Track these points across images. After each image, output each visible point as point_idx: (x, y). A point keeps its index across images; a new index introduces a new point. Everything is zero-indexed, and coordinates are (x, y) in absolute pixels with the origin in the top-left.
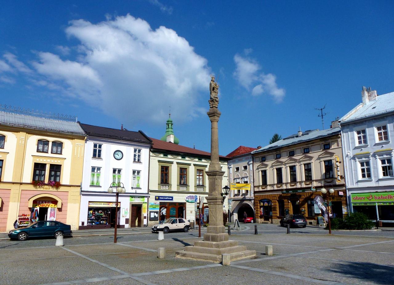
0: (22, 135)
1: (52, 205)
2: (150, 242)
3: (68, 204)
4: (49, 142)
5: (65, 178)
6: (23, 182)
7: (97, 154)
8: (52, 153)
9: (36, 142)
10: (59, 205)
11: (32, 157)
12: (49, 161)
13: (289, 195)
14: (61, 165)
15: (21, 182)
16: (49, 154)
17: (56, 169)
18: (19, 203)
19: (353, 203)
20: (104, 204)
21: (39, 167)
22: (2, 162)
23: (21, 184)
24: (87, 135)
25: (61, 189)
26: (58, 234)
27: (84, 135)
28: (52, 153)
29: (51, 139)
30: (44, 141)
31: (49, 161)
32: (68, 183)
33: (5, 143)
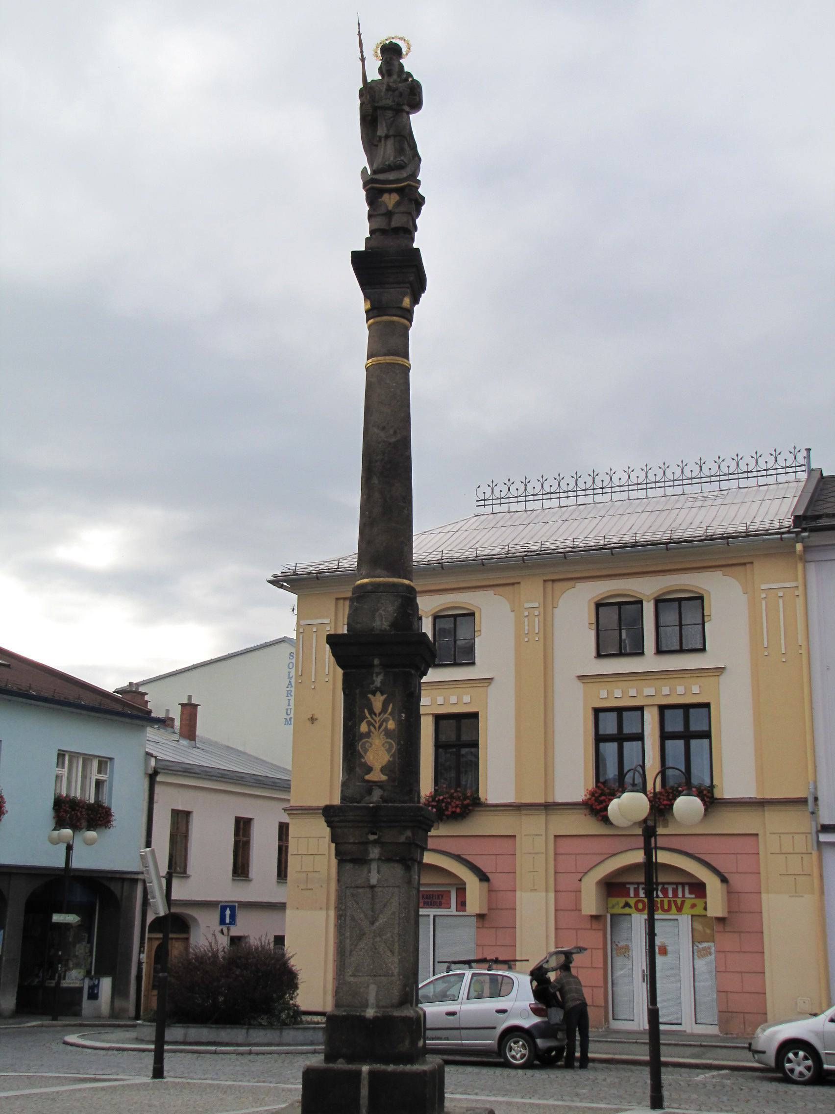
0: (531, 593)
1: (693, 906)
2: (28, 1096)
3: (764, 896)
4: (640, 602)
5: (736, 769)
6: (559, 799)
8: (659, 651)
9: (587, 614)
10: (716, 902)
11: (579, 685)
12: (649, 691)
13: (401, 841)
14: (475, 716)
15: (550, 800)
16: (649, 662)
17: (688, 725)
18: (552, 895)
19: (169, 909)
21: (614, 729)
22: (639, 712)
23: (549, 807)
24: (804, 530)
25: (482, 825)
26: (796, 1055)
27: (789, 532)
28: (659, 651)
29: (646, 588)
30: (620, 604)
31: (649, 691)
32: (749, 792)
33: (706, 625)
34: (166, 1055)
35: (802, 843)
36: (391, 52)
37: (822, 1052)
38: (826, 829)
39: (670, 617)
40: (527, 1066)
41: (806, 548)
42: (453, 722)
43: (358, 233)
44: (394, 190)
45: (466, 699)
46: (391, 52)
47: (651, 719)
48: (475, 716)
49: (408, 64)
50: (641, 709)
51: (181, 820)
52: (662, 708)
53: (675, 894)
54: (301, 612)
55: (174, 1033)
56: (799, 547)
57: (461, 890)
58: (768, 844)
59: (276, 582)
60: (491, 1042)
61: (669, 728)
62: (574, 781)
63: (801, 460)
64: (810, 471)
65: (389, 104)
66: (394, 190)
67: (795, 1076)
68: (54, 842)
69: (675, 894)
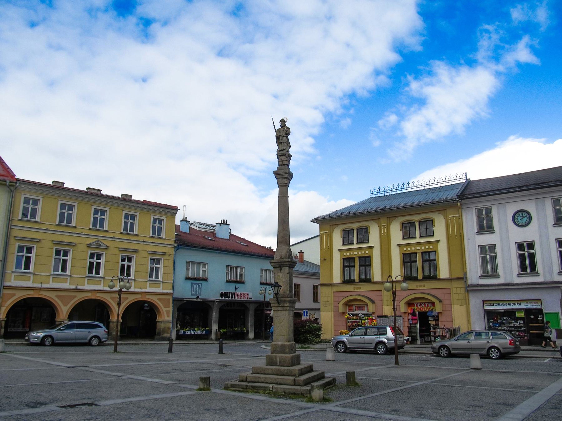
7: (486, 226)
12: (418, 248)
14: (369, 257)
20: (510, 304)
21: (408, 259)
34: (224, 345)
35: (463, 290)
36: (283, 122)
37: (101, 337)
38: (469, 286)
39: (424, 227)
40: (385, 354)
41: (461, 204)
42: (364, 259)
43: (275, 165)
44: (284, 155)
45: (367, 252)
46: (283, 122)
47: (419, 256)
48: (369, 257)
49: (287, 124)
50: (416, 253)
51: (297, 286)
52: (422, 253)
53: (428, 305)
54: (321, 229)
55: (227, 344)
56: (459, 204)
57: (368, 306)
58: (454, 291)
59: (314, 221)
60: (373, 346)
61: (424, 259)
62: (397, 271)
63: (464, 176)
64: (467, 179)
65: (283, 135)
66: (284, 155)
67: (442, 355)
68: (261, 294)
69: (428, 305)
